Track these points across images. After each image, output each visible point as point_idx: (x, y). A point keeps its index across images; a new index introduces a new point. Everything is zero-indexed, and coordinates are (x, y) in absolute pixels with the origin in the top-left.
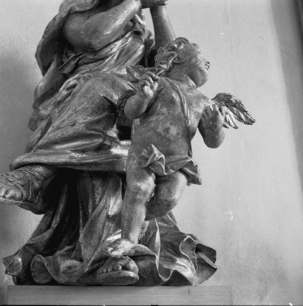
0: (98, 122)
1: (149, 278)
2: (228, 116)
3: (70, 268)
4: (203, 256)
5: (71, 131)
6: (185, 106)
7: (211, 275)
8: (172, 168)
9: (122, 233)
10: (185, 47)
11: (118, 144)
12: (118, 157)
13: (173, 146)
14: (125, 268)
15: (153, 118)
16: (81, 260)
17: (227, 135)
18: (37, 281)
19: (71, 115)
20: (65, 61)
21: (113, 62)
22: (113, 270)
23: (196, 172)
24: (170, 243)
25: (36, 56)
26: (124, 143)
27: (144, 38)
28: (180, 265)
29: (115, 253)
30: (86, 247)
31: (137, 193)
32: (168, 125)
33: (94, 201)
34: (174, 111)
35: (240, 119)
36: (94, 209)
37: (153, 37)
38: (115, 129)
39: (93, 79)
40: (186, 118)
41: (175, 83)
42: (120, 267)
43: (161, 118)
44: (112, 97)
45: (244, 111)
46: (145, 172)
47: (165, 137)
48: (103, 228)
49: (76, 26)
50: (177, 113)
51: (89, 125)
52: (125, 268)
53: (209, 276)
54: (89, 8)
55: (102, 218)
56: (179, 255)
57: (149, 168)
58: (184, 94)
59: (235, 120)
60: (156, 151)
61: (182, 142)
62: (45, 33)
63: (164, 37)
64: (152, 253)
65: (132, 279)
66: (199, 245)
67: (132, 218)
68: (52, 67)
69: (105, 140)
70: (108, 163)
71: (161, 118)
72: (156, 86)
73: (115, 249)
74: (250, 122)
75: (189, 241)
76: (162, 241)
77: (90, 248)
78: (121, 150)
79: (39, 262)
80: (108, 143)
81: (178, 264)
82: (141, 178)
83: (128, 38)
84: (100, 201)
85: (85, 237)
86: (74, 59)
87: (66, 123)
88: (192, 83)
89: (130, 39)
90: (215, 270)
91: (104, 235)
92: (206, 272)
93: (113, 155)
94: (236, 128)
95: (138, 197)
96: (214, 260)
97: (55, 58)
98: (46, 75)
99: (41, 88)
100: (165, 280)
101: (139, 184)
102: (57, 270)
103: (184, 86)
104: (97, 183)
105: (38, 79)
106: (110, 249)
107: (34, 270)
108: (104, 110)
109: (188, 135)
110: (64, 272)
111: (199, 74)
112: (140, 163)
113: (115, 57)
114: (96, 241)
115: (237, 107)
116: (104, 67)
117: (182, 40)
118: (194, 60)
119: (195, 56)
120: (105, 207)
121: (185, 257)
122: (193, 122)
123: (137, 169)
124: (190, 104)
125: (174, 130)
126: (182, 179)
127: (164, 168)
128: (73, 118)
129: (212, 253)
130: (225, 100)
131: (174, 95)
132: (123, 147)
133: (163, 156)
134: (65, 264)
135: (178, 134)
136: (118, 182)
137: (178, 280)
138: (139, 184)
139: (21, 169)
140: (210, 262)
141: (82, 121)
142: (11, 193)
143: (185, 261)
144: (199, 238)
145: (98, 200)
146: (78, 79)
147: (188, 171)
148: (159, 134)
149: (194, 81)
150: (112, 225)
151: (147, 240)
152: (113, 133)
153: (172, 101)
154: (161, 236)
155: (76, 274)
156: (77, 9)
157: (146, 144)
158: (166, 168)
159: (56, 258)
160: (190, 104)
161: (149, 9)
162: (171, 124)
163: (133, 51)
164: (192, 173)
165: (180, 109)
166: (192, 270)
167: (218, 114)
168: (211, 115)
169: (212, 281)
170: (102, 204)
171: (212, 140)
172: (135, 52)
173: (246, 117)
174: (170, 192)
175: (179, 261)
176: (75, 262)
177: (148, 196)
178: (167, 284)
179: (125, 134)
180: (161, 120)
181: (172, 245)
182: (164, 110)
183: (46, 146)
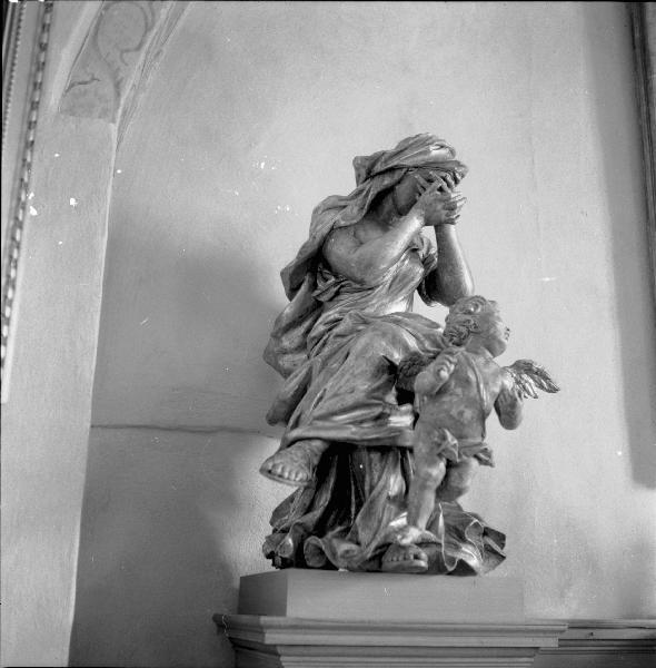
0: (378, 388)
1: (437, 567)
2: (527, 385)
3: (347, 552)
4: (491, 542)
5: (350, 400)
6: (482, 386)
8: (465, 454)
9: (408, 517)
12: (400, 431)
13: (467, 431)
14: (416, 557)
15: (446, 399)
16: (358, 544)
17: (526, 407)
18: (310, 564)
19: (348, 380)
20: (321, 285)
21: (384, 291)
22: (405, 559)
23: (490, 457)
27: (422, 253)
28: (466, 553)
31: (426, 480)
32: (462, 408)
33: (372, 479)
35: (541, 387)
36: (370, 492)
37: (434, 251)
38: (394, 391)
39: (370, 334)
40: (482, 399)
41: (470, 356)
42: (412, 557)
43: (455, 400)
44: (392, 356)
45: (546, 378)
46: (437, 458)
47: (459, 421)
48: (384, 509)
51: (371, 394)
52: (416, 557)
53: (496, 565)
54: (355, 221)
55: (383, 498)
57: (439, 451)
58: (480, 371)
59: (535, 389)
60: (449, 436)
61: (477, 427)
62: (300, 253)
63: (450, 260)
64: (438, 541)
66: (486, 528)
67: (420, 506)
68: (303, 288)
69: (384, 408)
70: (390, 438)
71: (455, 399)
72: (452, 368)
73: (404, 537)
74: (553, 390)
75: (476, 525)
77: (367, 531)
78: (401, 419)
80: (387, 411)
82: (432, 463)
83: (404, 260)
85: (363, 518)
86: (335, 284)
87: (342, 391)
88: (488, 354)
89: (406, 262)
90: (504, 558)
91: (385, 519)
92: (493, 560)
94: (536, 397)
97: (307, 278)
98: (294, 300)
99: (287, 315)
100: (450, 569)
101: (430, 470)
102: (334, 554)
103: (481, 360)
104: (375, 456)
105: (286, 305)
107: (308, 551)
108: (383, 372)
109: (483, 416)
110: (343, 557)
111: (497, 346)
112: (432, 449)
113: (387, 286)
114: (376, 524)
115: (541, 377)
116: (372, 299)
117: (479, 301)
119: (494, 325)
120: (385, 487)
121: (470, 543)
122: (488, 400)
124: (486, 384)
125: (468, 414)
126: (474, 463)
127: (456, 453)
128: (351, 384)
129: (501, 538)
130: (524, 367)
134: (344, 547)
135: (472, 418)
136: (397, 455)
137: (464, 569)
143: (470, 547)
148: (451, 417)
150: (393, 508)
151: (431, 526)
152: (391, 398)
153: (468, 381)
155: (355, 559)
156: (343, 223)
158: (460, 456)
159: (330, 541)
160: (486, 384)
161: (432, 227)
162: (466, 407)
165: (475, 390)
167: (516, 400)
169: (502, 571)
170: (381, 483)
172: (413, 279)
176: (354, 547)
178: (450, 574)
179: (405, 397)
180: (453, 403)
182: (459, 391)
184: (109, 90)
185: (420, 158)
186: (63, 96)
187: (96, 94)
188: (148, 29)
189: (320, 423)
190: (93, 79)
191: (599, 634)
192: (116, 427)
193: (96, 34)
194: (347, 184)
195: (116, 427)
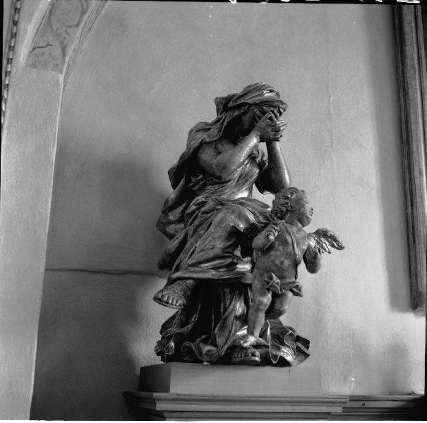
1: (266, 361)
3: (209, 351)
4: (300, 345)
5: (211, 254)
6: (295, 245)
7: (306, 359)
8: (285, 289)
9: (248, 330)
10: (296, 196)
11: (242, 260)
12: (243, 274)
13: (286, 274)
14: (253, 355)
15: (273, 253)
16: (216, 346)
17: (324, 259)
19: (211, 241)
21: (234, 184)
22: (245, 356)
23: (300, 290)
24: (277, 335)
25: (169, 172)
26: (245, 259)
27: (258, 160)
29: (245, 345)
30: (219, 337)
31: (260, 305)
32: (283, 259)
33: (225, 304)
34: (288, 249)
35: (333, 246)
36: (224, 313)
37: (266, 158)
41: (288, 225)
43: (278, 254)
45: (336, 240)
49: (207, 156)
50: (289, 250)
51: (225, 250)
52: (253, 355)
55: (233, 315)
56: (283, 344)
57: (268, 287)
58: (294, 236)
59: (329, 247)
62: (181, 158)
64: (266, 344)
65: (256, 361)
68: (182, 182)
72: (277, 233)
73: (245, 342)
74: (340, 248)
75: (291, 334)
76: (271, 334)
78: (244, 267)
79: (188, 347)
80: (235, 261)
81: (283, 352)
82: (263, 294)
83: (247, 164)
84: (230, 304)
86: (202, 179)
90: (308, 355)
91: (233, 330)
92: (301, 357)
93: (238, 272)
94: (330, 253)
95: (261, 307)
96: (308, 348)
98: (177, 189)
100: (275, 362)
101: (262, 299)
102: (201, 353)
103: (294, 229)
105: (170, 192)
106: (242, 342)
109: (296, 265)
110: (205, 354)
113: (236, 180)
117: (294, 190)
118: (302, 209)
119: (303, 206)
120: (234, 310)
121: (287, 346)
123: (261, 288)
124: (298, 244)
125: (287, 263)
126: (290, 294)
130: (322, 234)
131: (288, 238)
132: (246, 263)
133: (278, 281)
134: (207, 348)
137: (283, 363)
138: (262, 299)
139: (178, 282)
140: (305, 349)
141: (220, 245)
142: (179, 302)
143: (287, 349)
144: (297, 331)
145: (228, 303)
146: (206, 197)
147: (295, 290)
148: (277, 265)
149: (301, 223)
151: (262, 335)
152: (238, 253)
153: (286, 242)
154: (271, 329)
157: (268, 271)
158: (281, 289)
160: (298, 244)
161: (265, 143)
162: (285, 258)
163: (250, 175)
164: (297, 291)
165: (291, 248)
166: (292, 356)
167: (317, 254)
168: (312, 255)
169: (307, 364)
170: (231, 307)
171: (312, 266)
173: (338, 245)
174: (282, 304)
175: (284, 349)
176: (213, 348)
177: (267, 307)
181: (279, 337)
183: (196, 265)
184: (58, 52)
185: (258, 98)
186: (29, 56)
187: (50, 54)
188: (83, 13)
189: (192, 269)
190: (48, 45)
191: (368, 404)
192: (61, 270)
193: (50, 15)
194: (210, 114)
195: (61, 270)
